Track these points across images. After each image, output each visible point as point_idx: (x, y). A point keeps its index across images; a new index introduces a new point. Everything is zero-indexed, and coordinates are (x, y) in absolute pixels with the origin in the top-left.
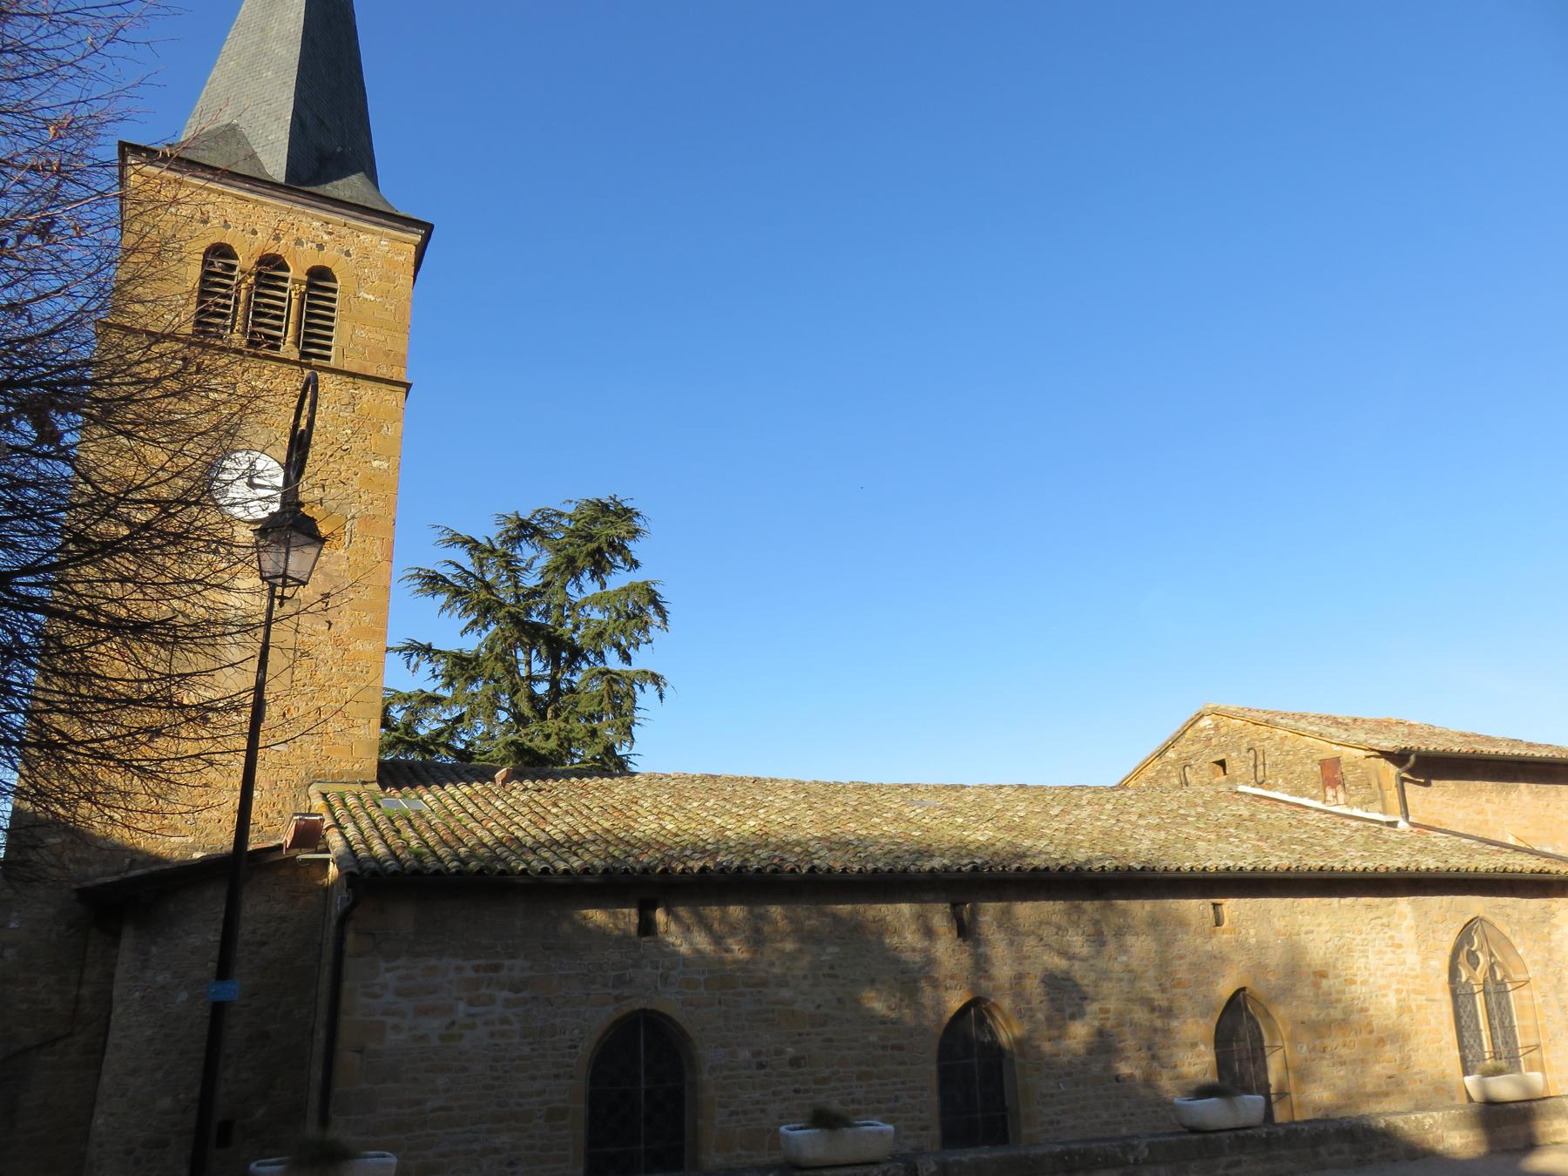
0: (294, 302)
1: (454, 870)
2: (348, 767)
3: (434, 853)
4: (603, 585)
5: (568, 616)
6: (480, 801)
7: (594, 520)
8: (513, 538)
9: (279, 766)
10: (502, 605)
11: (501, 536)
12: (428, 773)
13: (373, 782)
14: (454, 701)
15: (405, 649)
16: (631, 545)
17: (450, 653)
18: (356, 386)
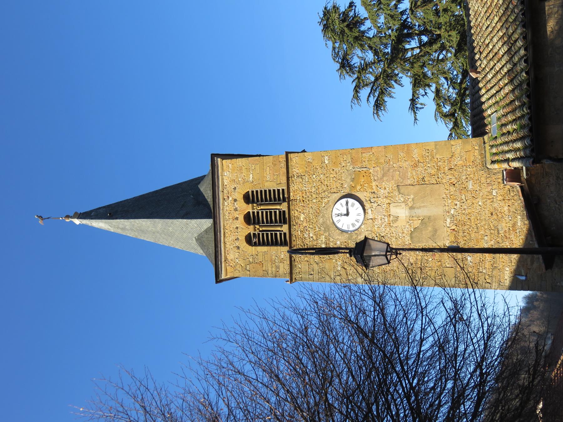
0: (262, 207)
1: (528, 111)
2: (477, 151)
3: (519, 118)
4: (366, 19)
5: (385, 34)
6: (489, 86)
7: (333, 31)
8: (350, 69)
9: (480, 184)
10: (384, 71)
11: (350, 75)
12: (476, 109)
13: (484, 139)
14: (437, 83)
15: (414, 111)
16: (342, 9)
17: (413, 89)
18: (293, 176)
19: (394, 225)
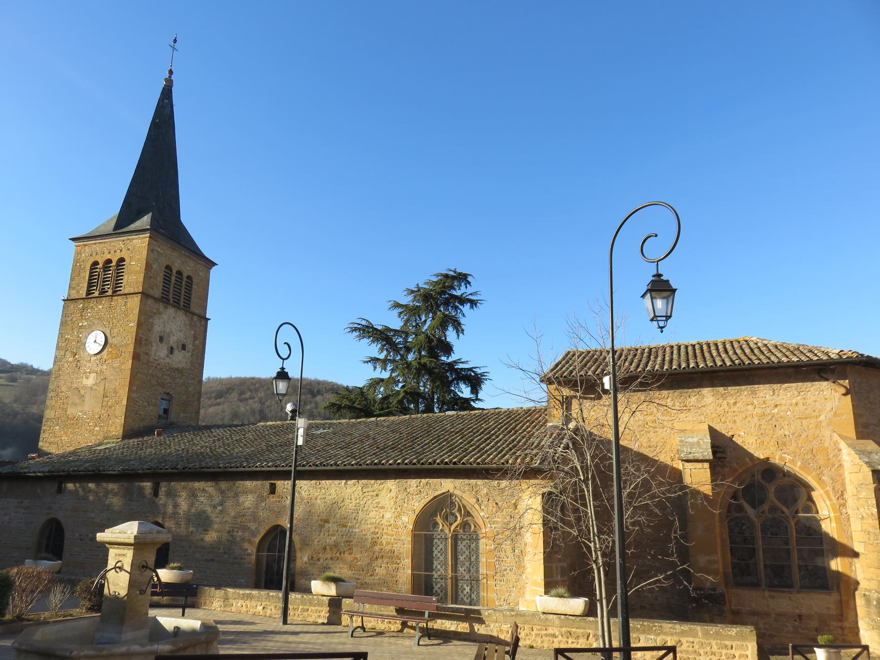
19: (84, 377)
